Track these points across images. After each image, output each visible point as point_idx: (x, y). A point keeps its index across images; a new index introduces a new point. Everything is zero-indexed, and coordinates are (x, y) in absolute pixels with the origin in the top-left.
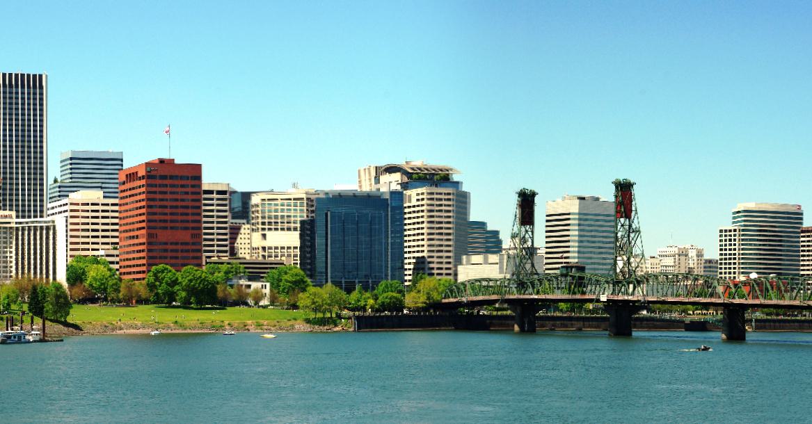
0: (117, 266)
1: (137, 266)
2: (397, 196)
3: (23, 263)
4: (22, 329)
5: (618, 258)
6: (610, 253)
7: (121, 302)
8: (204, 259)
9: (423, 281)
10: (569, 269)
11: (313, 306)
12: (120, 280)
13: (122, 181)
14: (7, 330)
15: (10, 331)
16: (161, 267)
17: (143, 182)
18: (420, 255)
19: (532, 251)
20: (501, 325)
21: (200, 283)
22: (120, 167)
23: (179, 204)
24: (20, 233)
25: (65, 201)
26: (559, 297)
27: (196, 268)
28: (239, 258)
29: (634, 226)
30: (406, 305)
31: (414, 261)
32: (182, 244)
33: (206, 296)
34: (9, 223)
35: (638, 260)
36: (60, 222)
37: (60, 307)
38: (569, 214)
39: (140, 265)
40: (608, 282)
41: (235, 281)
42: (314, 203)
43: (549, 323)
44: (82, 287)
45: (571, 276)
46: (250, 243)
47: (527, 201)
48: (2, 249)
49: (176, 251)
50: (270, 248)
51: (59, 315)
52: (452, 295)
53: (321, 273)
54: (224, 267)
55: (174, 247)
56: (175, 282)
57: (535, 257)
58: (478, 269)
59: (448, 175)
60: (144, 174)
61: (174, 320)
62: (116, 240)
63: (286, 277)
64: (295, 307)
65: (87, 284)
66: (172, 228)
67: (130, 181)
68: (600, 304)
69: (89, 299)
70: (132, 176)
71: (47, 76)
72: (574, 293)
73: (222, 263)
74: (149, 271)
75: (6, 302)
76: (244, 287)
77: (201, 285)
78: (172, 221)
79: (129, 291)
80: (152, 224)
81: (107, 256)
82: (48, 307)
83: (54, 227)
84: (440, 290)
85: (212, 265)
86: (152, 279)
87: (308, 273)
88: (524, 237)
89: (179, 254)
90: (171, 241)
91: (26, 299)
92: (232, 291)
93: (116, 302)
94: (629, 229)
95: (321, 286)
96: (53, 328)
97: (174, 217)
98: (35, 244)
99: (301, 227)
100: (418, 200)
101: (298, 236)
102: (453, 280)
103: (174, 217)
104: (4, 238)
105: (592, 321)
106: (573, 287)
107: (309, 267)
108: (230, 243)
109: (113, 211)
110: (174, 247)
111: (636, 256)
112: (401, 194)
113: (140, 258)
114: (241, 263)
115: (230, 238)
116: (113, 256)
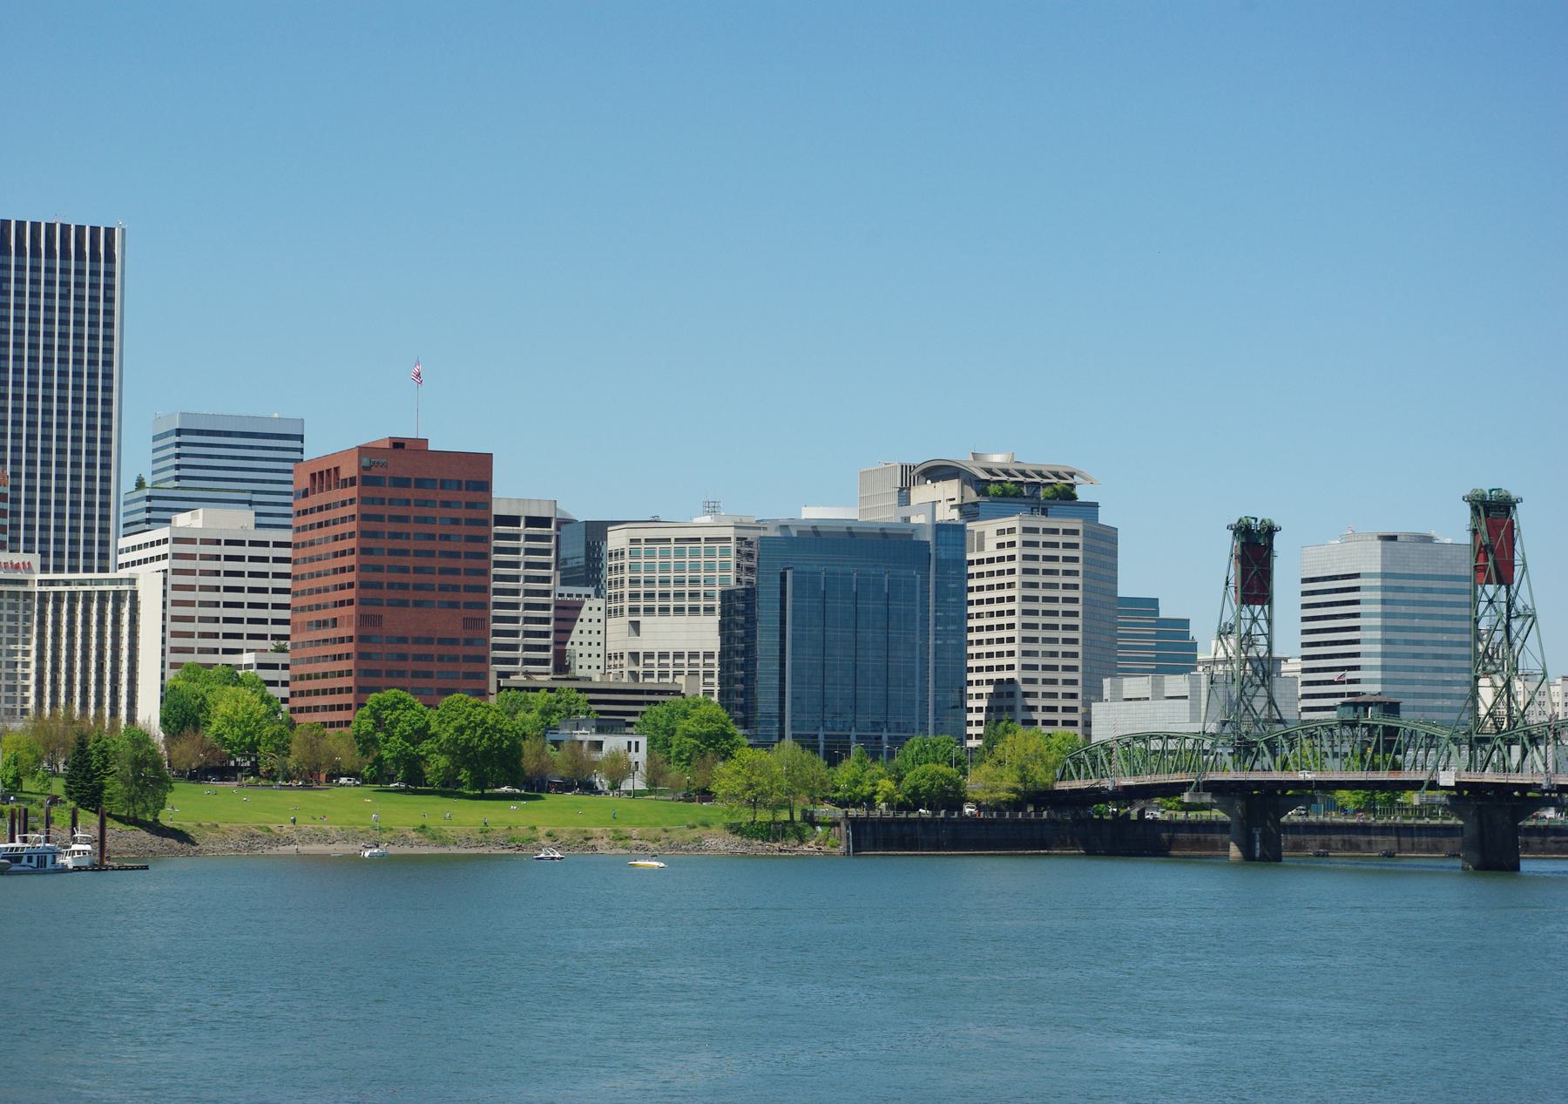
0: (284, 692)
2: (951, 535)
3: (55, 681)
4: (48, 840)
5: (1482, 682)
6: (1461, 670)
7: (292, 779)
8: (493, 679)
9: (1009, 738)
10: (1361, 709)
11: (748, 794)
12: (292, 725)
13: (302, 488)
14: (13, 840)
15: (18, 844)
16: (389, 695)
17: (352, 492)
18: (1005, 675)
19: (1267, 668)
20: (1196, 844)
22: (296, 455)
23: (438, 546)
24: (50, 607)
25: (162, 532)
26: (1336, 777)
27: (474, 700)
28: (577, 679)
29: (1519, 604)
30: (970, 795)
31: (990, 689)
32: (441, 641)
33: (495, 768)
34: (24, 582)
35: (1532, 686)
36: (150, 586)
37: (144, 787)
38: (1357, 576)
39: (340, 691)
40: (1456, 741)
41: (564, 733)
42: (754, 550)
43: (1314, 841)
44: (198, 739)
45: (1364, 725)
46: (604, 642)
47: (1255, 551)
48: (4, 647)
49: (427, 658)
50: (649, 655)
51: (140, 806)
52: (1078, 772)
53: (770, 715)
54: (541, 699)
55: (424, 649)
56: (422, 734)
57: (1277, 681)
58: (1142, 713)
59: (1072, 486)
60: (355, 473)
61: (420, 823)
63: (685, 724)
64: (706, 795)
66: (417, 604)
67: (321, 490)
68: (1438, 793)
69: (220, 771)
70: (324, 477)
72: (1375, 768)
73: (536, 690)
74: (361, 705)
75: (11, 773)
76: (585, 745)
79: (312, 752)
80: (371, 593)
81: (261, 666)
82: (114, 787)
83: (134, 594)
84: (1050, 760)
86: (367, 725)
87: (740, 714)
88: (1248, 633)
89: (435, 667)
90: (416, 635)
91: (61, 767)
92: (556, 755)
94: (1509, 610)
95: (767, 745)
96: (123, 838)
99: (722, 607)
101: (716, 628)
102: (1080, 737)
104: (11, 618)
105: (1420, 835)
106: (1370, 751)
107: (741, 700)
108: (556, 643)
109: (276, 591)
110: (424, 649)
111: (1527, 677)
112: (960, 529)
113: (340, 674)
114: (580, 691)
115: (556, 631)
116: (274, 667)
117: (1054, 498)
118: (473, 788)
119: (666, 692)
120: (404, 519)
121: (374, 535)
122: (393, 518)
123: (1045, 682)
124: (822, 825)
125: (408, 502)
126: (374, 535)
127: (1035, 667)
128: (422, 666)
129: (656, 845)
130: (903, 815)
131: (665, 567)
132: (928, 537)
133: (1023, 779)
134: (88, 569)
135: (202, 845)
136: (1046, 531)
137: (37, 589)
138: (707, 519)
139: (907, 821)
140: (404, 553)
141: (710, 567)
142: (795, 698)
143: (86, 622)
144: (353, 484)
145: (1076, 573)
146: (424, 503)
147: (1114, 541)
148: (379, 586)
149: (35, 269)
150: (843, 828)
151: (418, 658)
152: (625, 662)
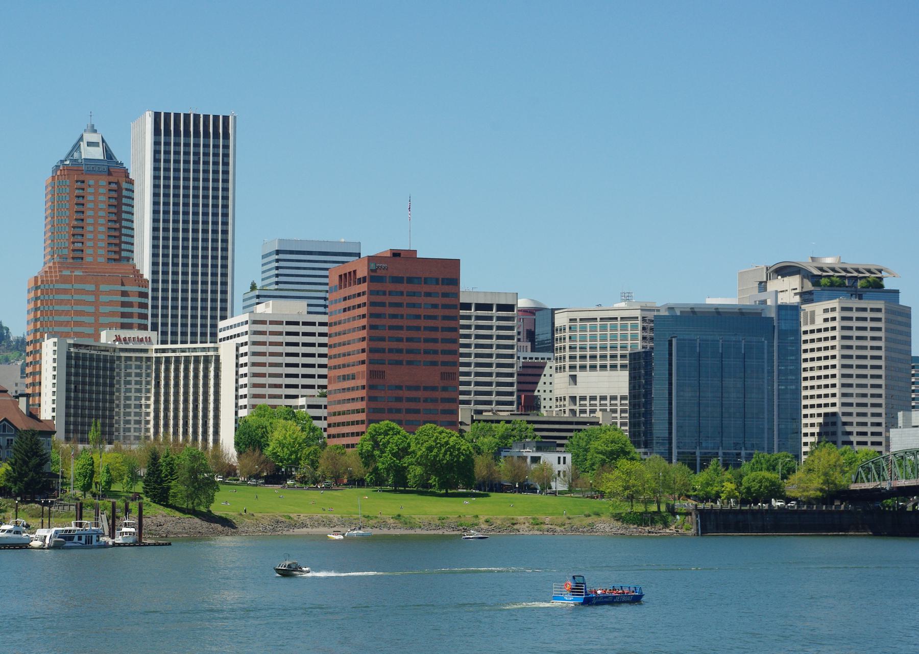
0: (322, 424)
1: (353, 423)
2: (790, 313)
3: (166, 417)
7: (318, 482)
11: (627, 493)
12: (324, 445)
16: (384, 424)
17: (364, 287)
21: (445, 454)
24: (163, 367)
31: (821, 420)
32: (426, 388)
33: (455, 475)
34: (146, 351)
50: (583, 398)
54: (501, 428)
55: (414, 394)
56: (404, 451)
59: (881, 279)
60: (366, 274)
61: (397, 513)
62: (324, 382)
65: (268, 451)
66: (410, 363)
69: (276, 477)
71: (235, 117)
73: (498, 422)
76: (529, 460)
77: (448, 457)
78: (409, 351)
80: (377, 356)
81: (310, 407)
82: (178, 488)
83: (217, 358)
85: (481, 425)
86: (368, 446)
89: (421, 406)
93: (310, 482)
97: (414, 345)
98: (186, 386)
100: (826, 320)
103: (414, 345)
110: (414, 394)
114: (529, 422)
115: (518, 383)
116: (319, 407)
117: (867, 287)
118: (440, 488)
119: (585, 423)
120: (399, 305)
121: (378, 316)
122: (392, 305)
123: (859, 414)
124: (680, 514)
125: (402, 293)
126: (378, 316)
127: (851, 405)
128: (413, 405)
129: (562, 529)
130: (747, 508)
131: (593, 338)
132: (773, 315)
133: (826, 482)
134: (173, 342)
135: (240, 530)
136: (858, 309)
137: (154, 355)
138: (623, 305)
139: (753, 512)
140: (400, 328)
141: (624, 337)
142: (679, 427)
143: (186, 377)
144: (364, 282)
145: (880, 339)
146: (414, 294)
147: (909, 316)
148: (382, 351)
149: (177, 144)
150: (694, 516)
151: (409, 400)
152: (567, 402)
